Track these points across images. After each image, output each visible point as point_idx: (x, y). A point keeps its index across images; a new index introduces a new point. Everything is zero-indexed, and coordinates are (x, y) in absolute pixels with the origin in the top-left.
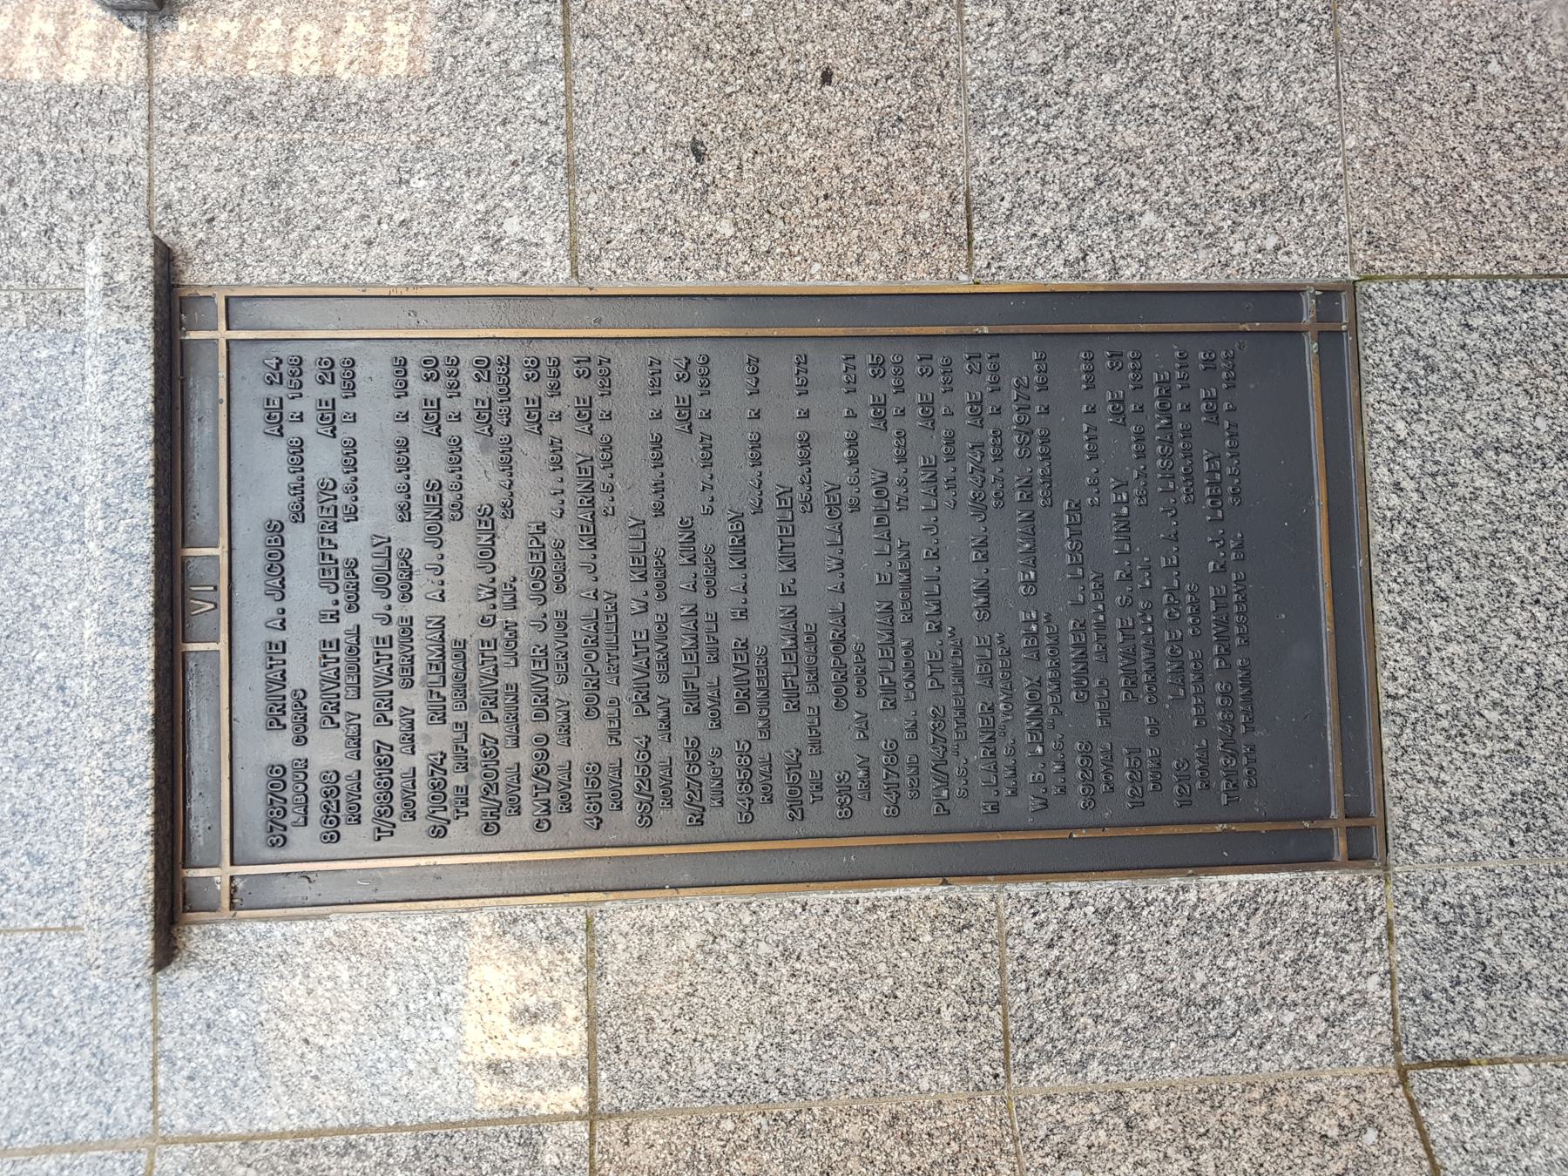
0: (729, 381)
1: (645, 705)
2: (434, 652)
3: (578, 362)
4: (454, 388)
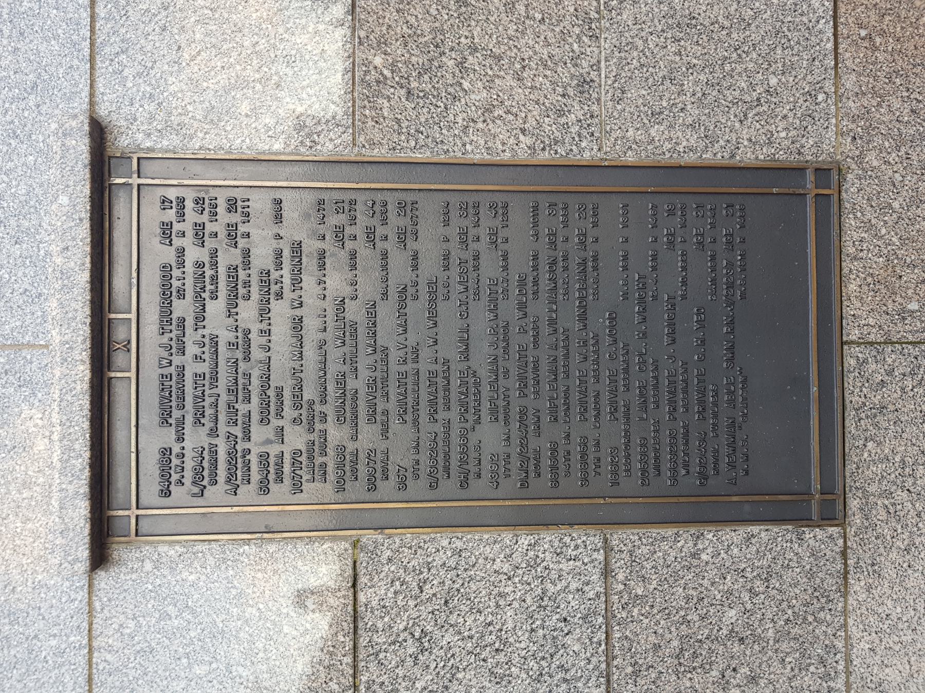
0: (519, 217)
1: (435, 416)
2: (231, 381)
3: (336, 203)
4: (181, 215)
